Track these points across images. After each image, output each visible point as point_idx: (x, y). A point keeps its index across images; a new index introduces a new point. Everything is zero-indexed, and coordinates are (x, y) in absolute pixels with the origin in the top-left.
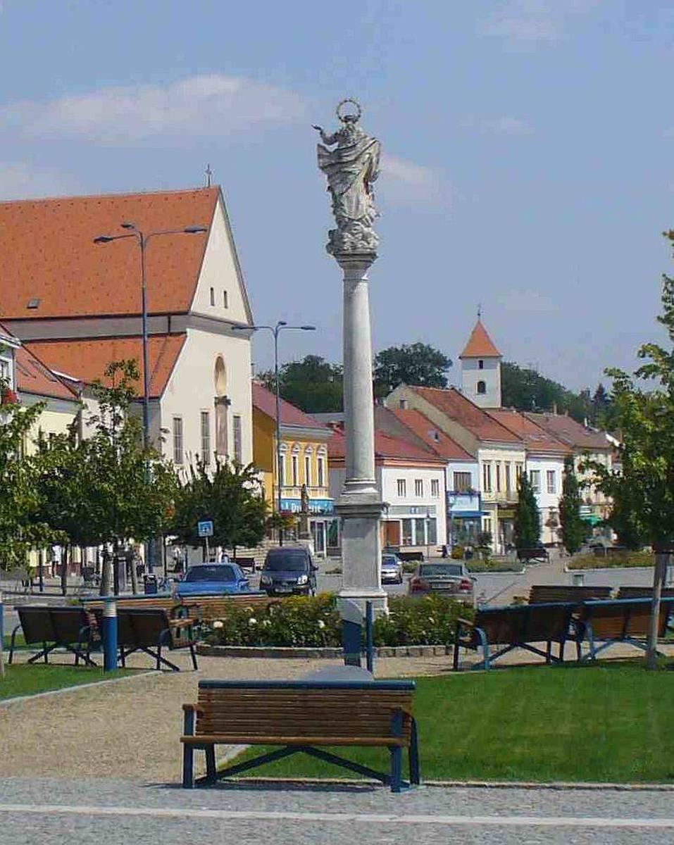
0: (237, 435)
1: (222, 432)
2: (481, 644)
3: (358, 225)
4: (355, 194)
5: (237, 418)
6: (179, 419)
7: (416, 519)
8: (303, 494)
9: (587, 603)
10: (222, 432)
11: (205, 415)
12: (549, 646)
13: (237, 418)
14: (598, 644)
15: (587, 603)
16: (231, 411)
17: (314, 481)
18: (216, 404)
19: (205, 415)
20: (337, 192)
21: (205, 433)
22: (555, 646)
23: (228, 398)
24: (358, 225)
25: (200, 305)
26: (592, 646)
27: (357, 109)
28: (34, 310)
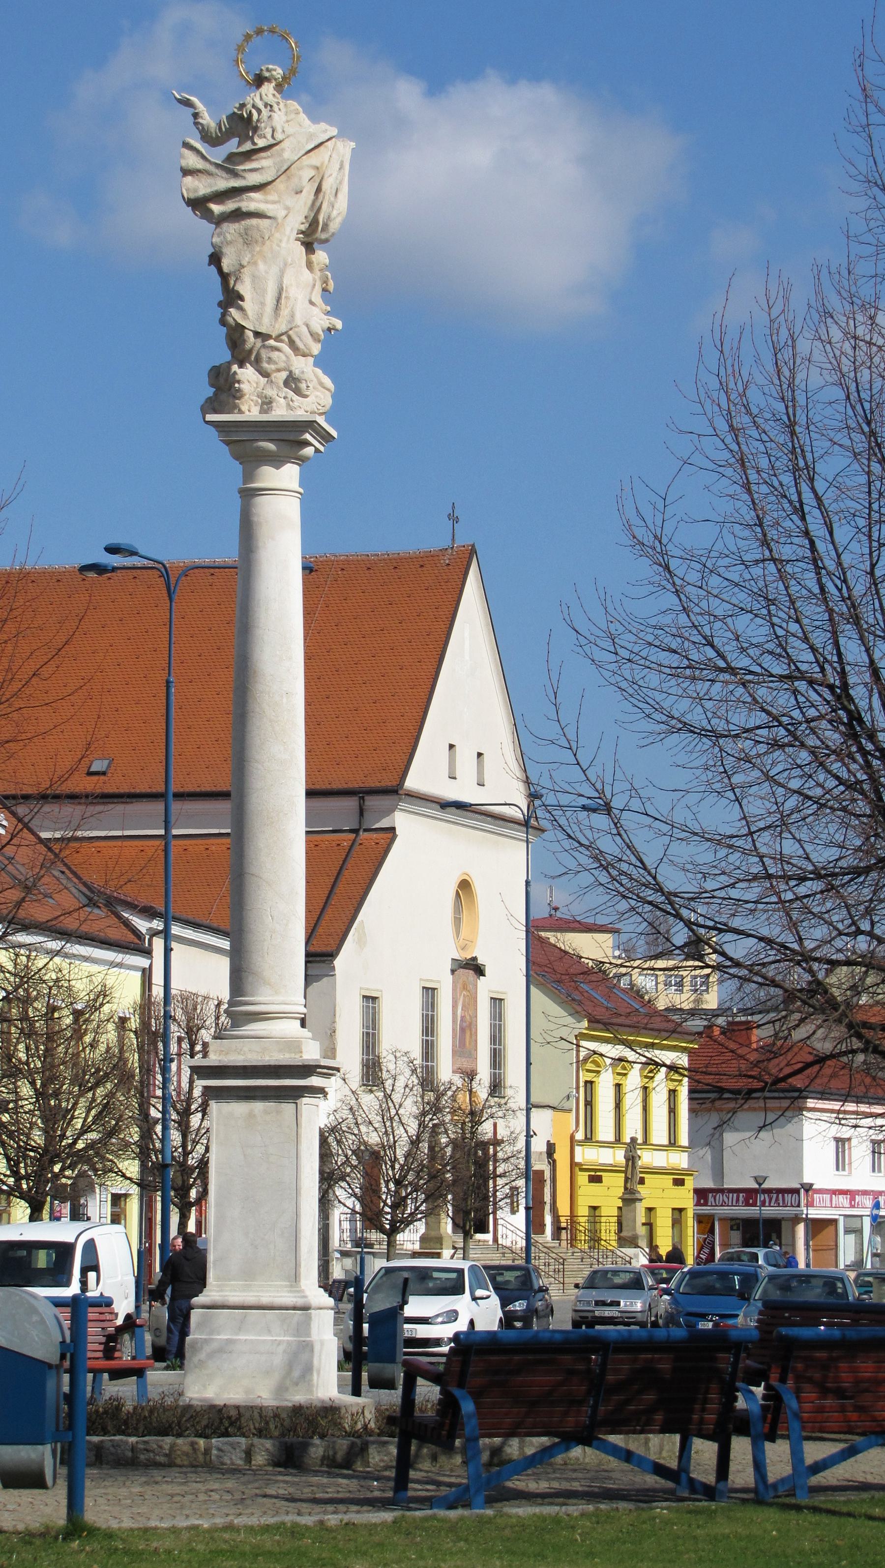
0: (497, 1037)
1: (465, 1031)
2: (65, 1394)
3: (277, 349)
4: (275, 270)
5: (497, 1003)
6: (374, 999)
7: (846, 1216)
8: (631, 1159)
9: (784, 1331)
10: (465, 1031)
11: (430, 993)
12: (685, 1447)
13: (497, 1003)
14: (814, 1452)
15: (784, 1331)
16: (485, 988)
17: (659, 1133)
18: (453, 971)
19: (430, 993)
20: (227, 264)
21: (429, 1027)
22: (705, 1451)
23: (480, 961)
24: (277, 349)
25: (412, 782)
26: (797, 1455)
27: (256, 40)
28: (102, 777)
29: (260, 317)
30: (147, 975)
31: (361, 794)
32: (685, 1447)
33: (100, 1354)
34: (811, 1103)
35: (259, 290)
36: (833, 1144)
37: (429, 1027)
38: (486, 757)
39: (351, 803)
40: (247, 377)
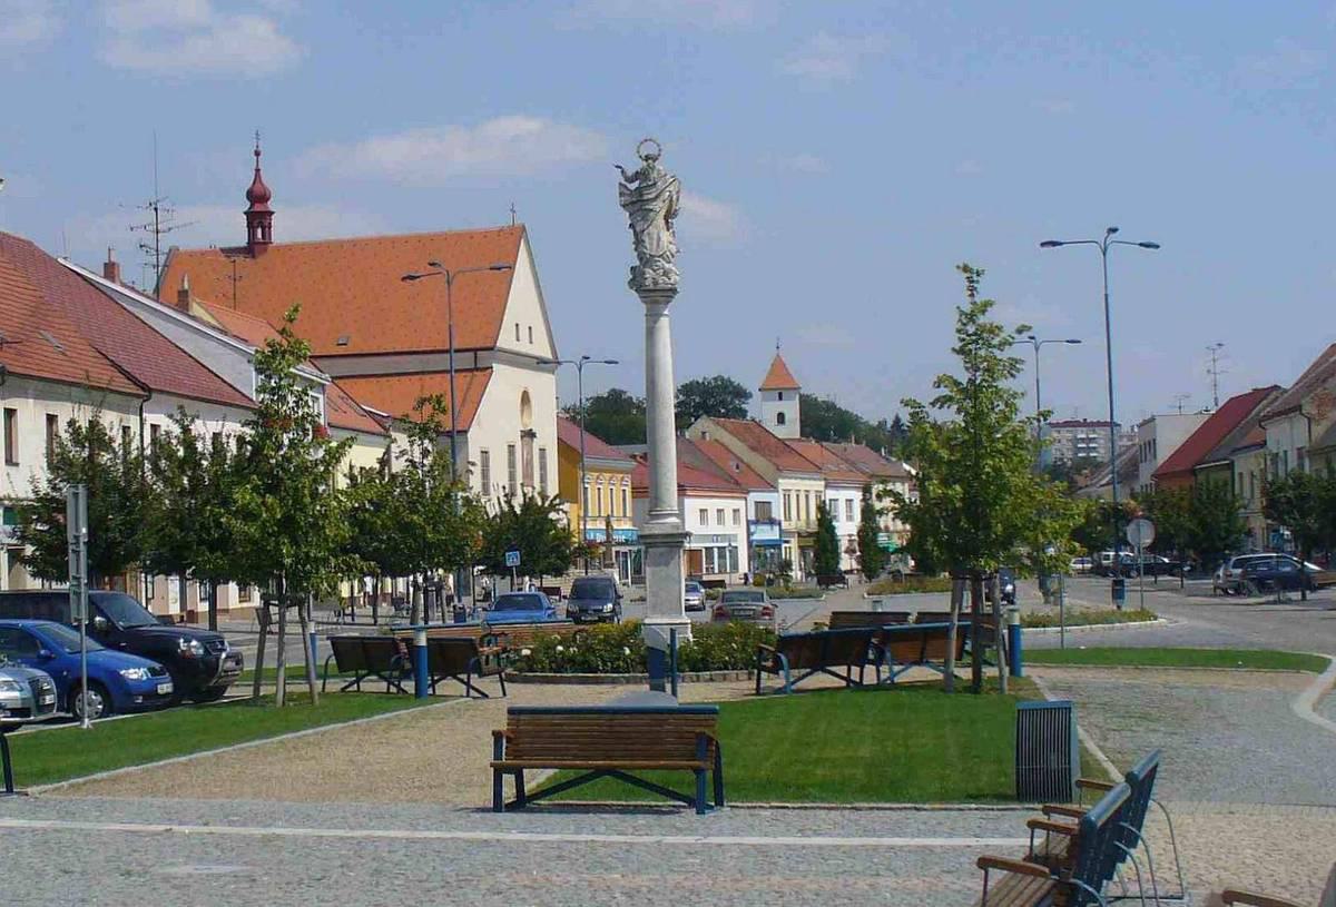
0: (543, 467)
1: (528, 465)
5: (542, 450)
6: (486, 452)
8: (608, 524)
9: (885, 627)
10: (528, 465)
11: (511, 447)
12: (849, 670)
13: (542, 450)
14: (896, 668)
15: (885, 627)
16: (537, 444)
17: (618, 512)
19: (511, 447)
21: (512, 465)
22: (855, 670)
25: (505, 340)
26: (891, 670)
29: (651, 250)
30: (960, 609)
31: (475, 350)
32: (849, 670)
33: (754, 692)
34: (689, 493)
35: (651, 239)
36: (699, 513)
37: (512, 465)
38: (520, 327)
39: (472, 354)
40: (649, 273)
